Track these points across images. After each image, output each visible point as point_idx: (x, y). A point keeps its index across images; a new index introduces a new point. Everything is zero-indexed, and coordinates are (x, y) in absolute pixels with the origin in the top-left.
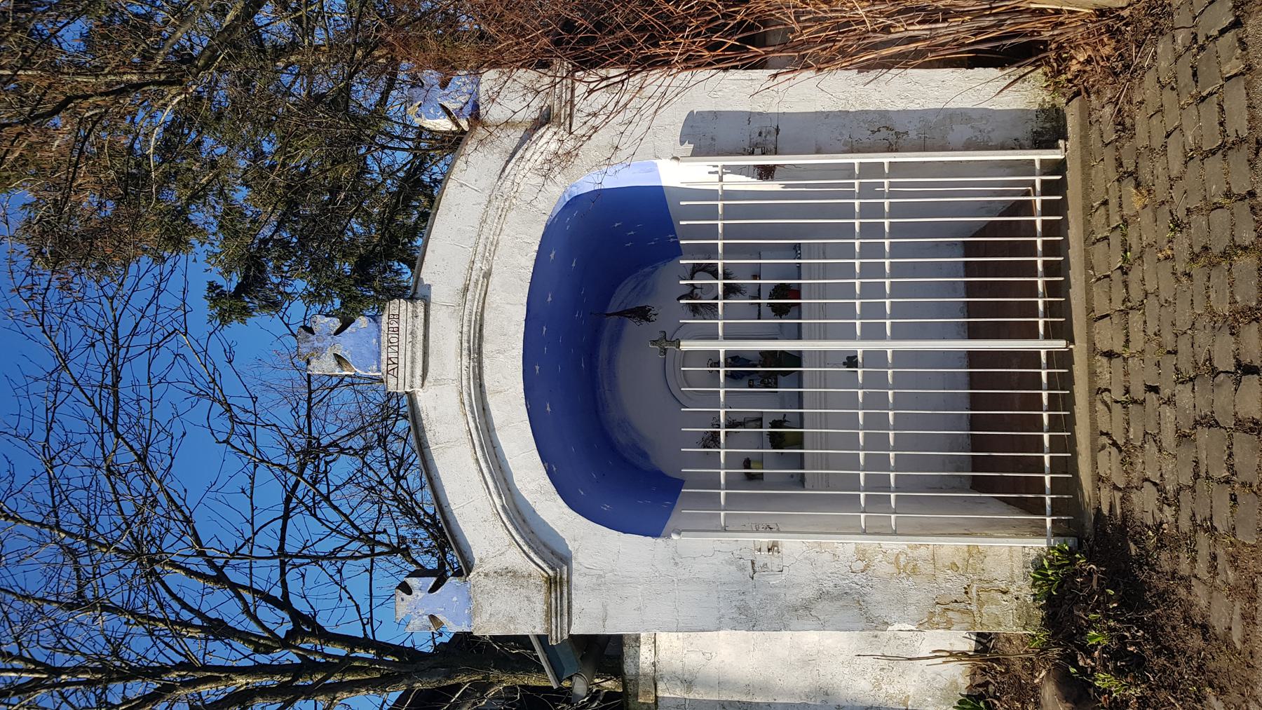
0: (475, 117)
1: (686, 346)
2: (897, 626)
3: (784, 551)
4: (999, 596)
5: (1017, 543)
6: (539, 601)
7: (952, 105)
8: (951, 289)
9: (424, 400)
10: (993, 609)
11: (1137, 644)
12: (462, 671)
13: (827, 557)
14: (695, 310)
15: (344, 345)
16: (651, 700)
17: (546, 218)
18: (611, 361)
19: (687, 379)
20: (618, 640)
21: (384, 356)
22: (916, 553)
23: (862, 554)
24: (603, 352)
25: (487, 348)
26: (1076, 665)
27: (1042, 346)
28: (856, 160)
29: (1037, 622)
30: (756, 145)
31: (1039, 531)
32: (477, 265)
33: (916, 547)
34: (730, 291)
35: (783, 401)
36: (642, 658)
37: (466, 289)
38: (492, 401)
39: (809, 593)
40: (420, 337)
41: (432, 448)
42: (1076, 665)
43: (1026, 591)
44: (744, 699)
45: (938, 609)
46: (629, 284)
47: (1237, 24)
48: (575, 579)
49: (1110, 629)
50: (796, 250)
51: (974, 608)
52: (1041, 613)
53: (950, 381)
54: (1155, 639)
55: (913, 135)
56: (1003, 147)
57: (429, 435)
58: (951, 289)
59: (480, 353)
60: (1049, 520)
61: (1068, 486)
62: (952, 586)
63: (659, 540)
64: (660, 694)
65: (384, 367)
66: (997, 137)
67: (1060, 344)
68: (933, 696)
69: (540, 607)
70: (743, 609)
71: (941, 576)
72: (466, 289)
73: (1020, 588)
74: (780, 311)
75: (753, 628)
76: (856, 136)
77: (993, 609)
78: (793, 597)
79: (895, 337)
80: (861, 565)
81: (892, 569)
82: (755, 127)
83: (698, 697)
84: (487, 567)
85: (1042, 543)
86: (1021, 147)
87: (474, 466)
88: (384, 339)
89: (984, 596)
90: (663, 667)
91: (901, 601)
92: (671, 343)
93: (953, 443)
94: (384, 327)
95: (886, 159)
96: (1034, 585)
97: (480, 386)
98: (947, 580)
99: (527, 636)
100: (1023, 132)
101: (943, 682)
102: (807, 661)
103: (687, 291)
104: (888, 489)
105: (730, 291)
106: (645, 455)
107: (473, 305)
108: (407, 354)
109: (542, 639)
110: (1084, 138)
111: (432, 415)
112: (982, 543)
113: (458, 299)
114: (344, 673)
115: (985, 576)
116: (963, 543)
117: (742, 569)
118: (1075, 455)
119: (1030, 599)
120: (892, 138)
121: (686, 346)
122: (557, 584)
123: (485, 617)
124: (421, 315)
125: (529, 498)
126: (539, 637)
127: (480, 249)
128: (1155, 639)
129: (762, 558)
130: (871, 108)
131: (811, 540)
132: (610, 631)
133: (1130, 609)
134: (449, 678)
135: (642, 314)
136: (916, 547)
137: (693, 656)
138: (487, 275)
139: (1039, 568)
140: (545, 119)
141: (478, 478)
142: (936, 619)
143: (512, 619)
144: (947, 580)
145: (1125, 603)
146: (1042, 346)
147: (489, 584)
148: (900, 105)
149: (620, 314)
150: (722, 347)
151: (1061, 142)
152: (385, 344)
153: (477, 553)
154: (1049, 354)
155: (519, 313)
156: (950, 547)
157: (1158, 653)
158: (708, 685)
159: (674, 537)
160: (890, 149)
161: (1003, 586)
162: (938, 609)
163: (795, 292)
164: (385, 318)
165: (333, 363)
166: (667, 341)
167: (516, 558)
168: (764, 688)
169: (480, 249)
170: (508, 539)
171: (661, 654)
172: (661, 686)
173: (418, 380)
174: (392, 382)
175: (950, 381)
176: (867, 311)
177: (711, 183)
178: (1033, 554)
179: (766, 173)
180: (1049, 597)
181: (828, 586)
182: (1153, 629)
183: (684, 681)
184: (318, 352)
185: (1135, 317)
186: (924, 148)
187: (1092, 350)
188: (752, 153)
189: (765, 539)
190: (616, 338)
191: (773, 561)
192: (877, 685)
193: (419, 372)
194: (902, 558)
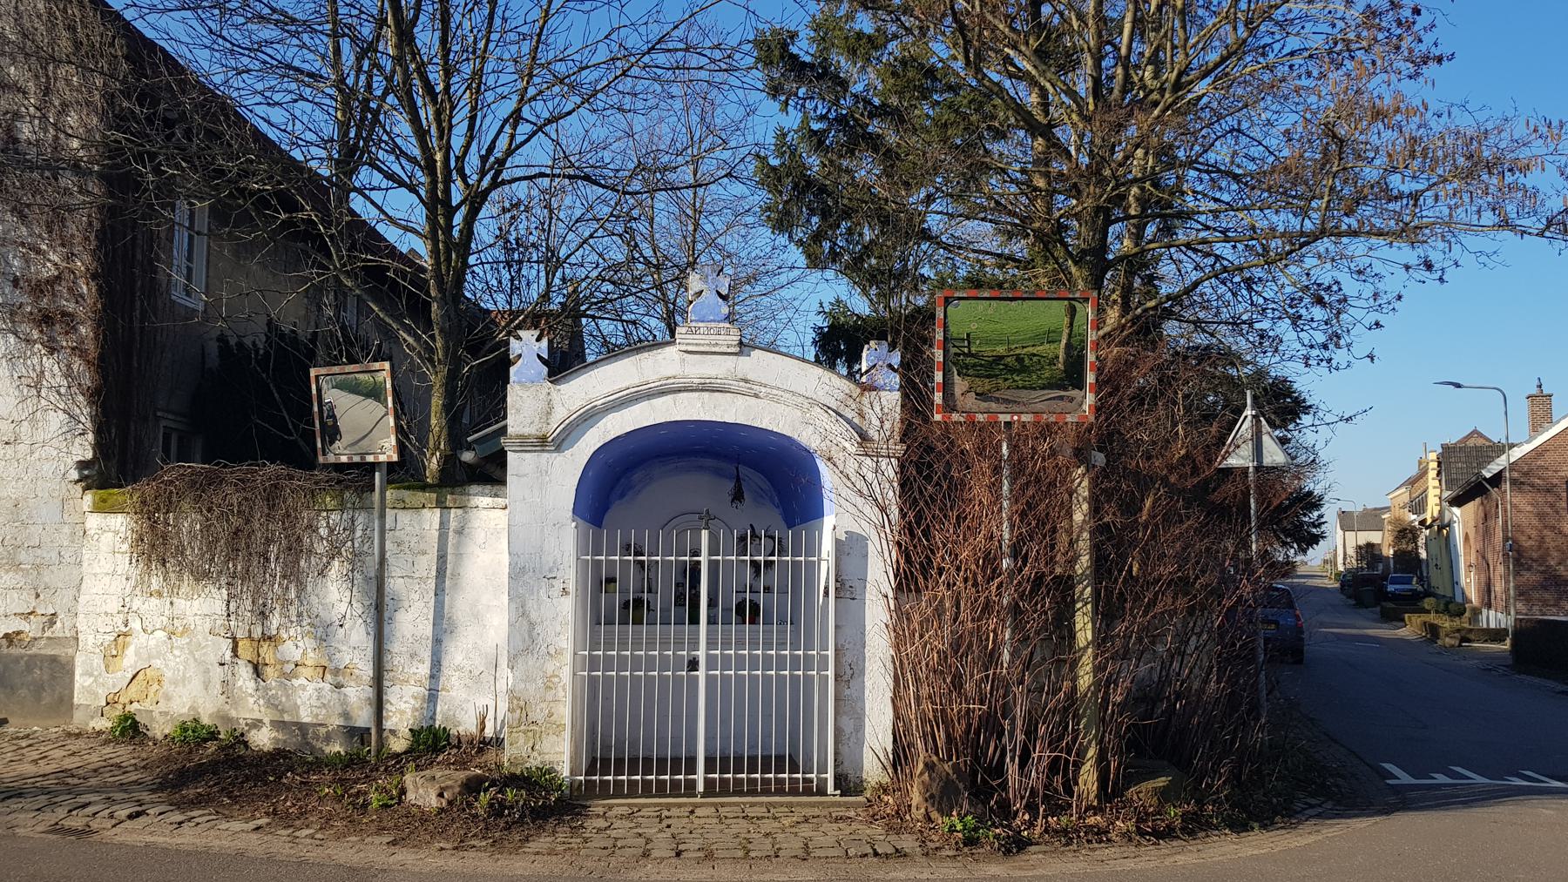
0: (865, 388)
1: (705, 534)
2: (510, 675)
3: (563, 599)
4: (531, 744)
5: (566, 758)
6: (531, 430)
7: (867, 720)
8: (753, 746)
9: (670, 351)
10: (521, 741)
11: (509, 815)
12: (447, 342)
13: (558, 629)
14: (742, 539)
15: (710, 297)
16: (448, 504)
17: (796, 437)
18: (701, 468)
19: (681, 533)
20: (502, 482)
21: (701, 324)
22: (560, 689)
23: (559, 652)
24: (709, 462)
25: (706, 395)
26: (490, 786)
27: (700, 777)
28: (831, 653)
29: (513, 770)
30: (843, 584)
31: (572, 773)
32: (763, 390)
33: (564, 690)
34: (756, 565)
35: (666, 611)
36: (481, 499)
37: (746, 381)
38: (669, 398)
39: (534, 616)
40: (713, 349)
41: (637, 357)
42: (490, 786)
43: (533, 763)
44: (448, 572)
45: (522, 703)
46: (766, 485)
47: (876, 854)
48: (546, 455)
49: (517, 802)
50: (782, 622)
51: (522, 727)
52: (518, 772)
53: (677, 743)
54: (513, 823)
55: (847, 692)
56: (836, 753)
57: (646, 354)
58: (753, 746)
59: (702, 390)
60: (582, 778)
61: (604, 791)
62: (537, 714)
63: (571, 514)
64: (453, 511)
65: (694, 324)
66: (844, 750)
67: (700, 788)
68: (449, 710)
69: (526, 431)
70: (523, 570)
71: (544, 705)
72: (746, 381)
73: (535, 759)
74: (740, 607)
75: (510, 577)
76: (848, 654)
77: (521, 741)
78: (530, 604)
79: (708, 677)
80: (553, 652)
81: (549, 673)
82: (856, 584)
83: (450, 538)
84: (554, 395)
85: (566, 772)
86: (836, 766)
87: (624, 386)
88: (713, 324)
89: (530, 734)
90: (473, 514)
91: (528, 679)
92: (707, 524)
93: (634, 744)
94: (722, 325)
95: (831, 673)
96: (537, 768)
97: (679, 391)
98: (541, 710)
99: (505, 417)
100: (847, 768)
101: (460, 716)
102: (477, 617)
103: (757, 532)
104: (605, 670)
105: (756, 565)
106: (622, 496)
107: (735, 385)
108: (702, 340)
109: (503, 431)
110: (839, 804)
111: (660, 357)
112: (567, 734)
113: (740, 376)
114: (444, 242)
115: (544, 735)
116: (567, 721)
117: (551, 571)
118: (627, 797)
119: (528, 765)
120: (845, 678)
121: (705, 534)
122: (542, 443)
123: (520, 393)
124: (729, 350)
125: (601, 424)
126: (505, 428)
127: (775, 392)
128: (513, 823)
129: (558, 585)
130: (867, 664)
131: (570, 618)
132: (509, 479)
133: (531, 812)
134: (441, 331)
135: (738, 496)
136: (564, 690)
137: (483, 534)
138: (756, 396)
139: (549, 771)
140: (864, 437)
141: (616, 388)
142: (515, 702)
143: (518, 411)
144: (541, 710)
145: (533, 810)
146: (700, 777)
147: (543, 395)
148: (868, 684)
149: (738, 479)
150: (703, 559)
151: (838, 792)
152: (709, 325)
153: (563, 387)
154: (694, 781)
155: (729, 418)
156: (564, 712)
157: (507, 823)
158: (458, 546)
159: (574, 524)
160: (837, 677)
161: (537, 747)
162: (522, 703)
163: (753, 621)
164: (728, 325)
165: (697, 290)
166: (708, 519)
167: (560, 415)
168: (455, 586)
169: (775, 392)
170: (574, 408)
171: (484, 512)
172: (460, 512)
173: (684, 348)
174: (683, 330)
175: (677, 743)
176: (726, 659)
177: (824, 555)
178: (559, 768)
179: (826, 593)
180: (529, 778)
181: (538, 629)
182: (520, 822)
183: (463, 528)
184: (704, 279)
185: (717, 821)
186: (837, 700)
187: (696, 806)
188: (837, 581)
189: (571, 587)
190: (718, 473)
191: (556, 591)
192: (459, 668)
193: (690, 348)
194: (556, 680)
